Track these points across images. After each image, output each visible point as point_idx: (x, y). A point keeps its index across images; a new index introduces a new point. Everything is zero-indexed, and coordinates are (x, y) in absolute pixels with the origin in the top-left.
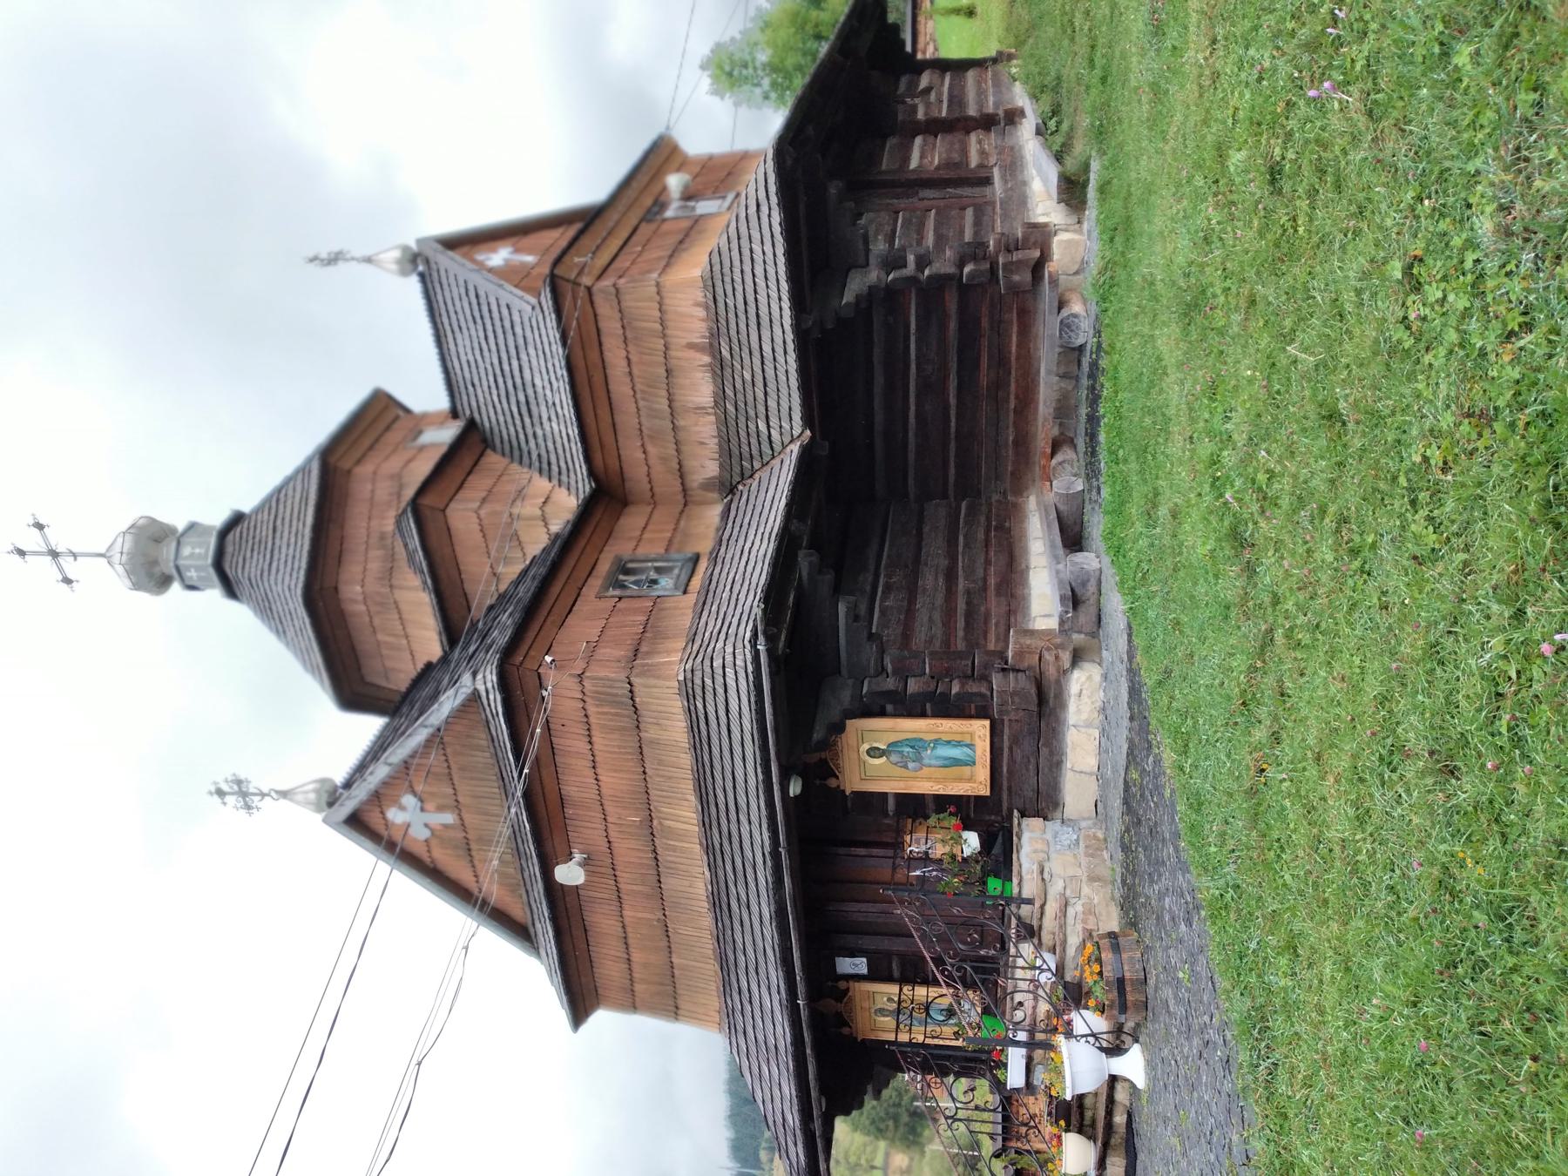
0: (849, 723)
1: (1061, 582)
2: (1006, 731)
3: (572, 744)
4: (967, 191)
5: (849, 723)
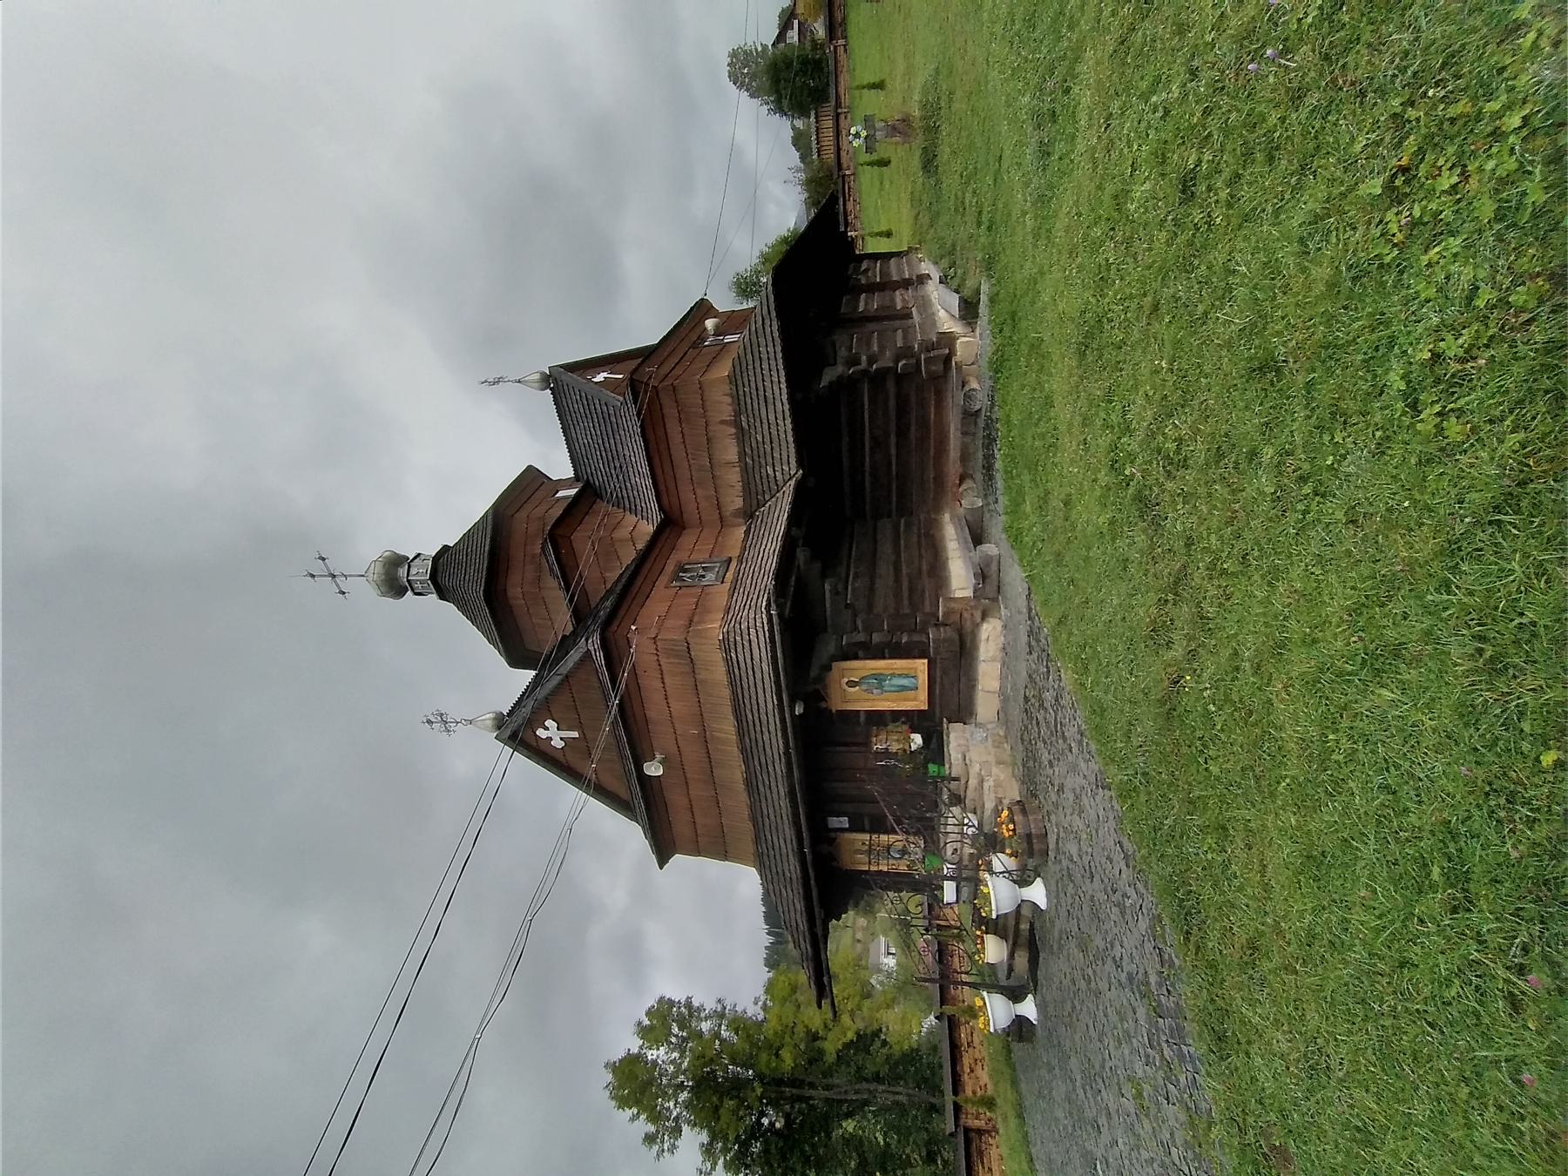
0: (834, 664)
1: (973, 563)
2: (938, 665)
3: (650, 683)
4: (897, 323)
5: (834, 664)
